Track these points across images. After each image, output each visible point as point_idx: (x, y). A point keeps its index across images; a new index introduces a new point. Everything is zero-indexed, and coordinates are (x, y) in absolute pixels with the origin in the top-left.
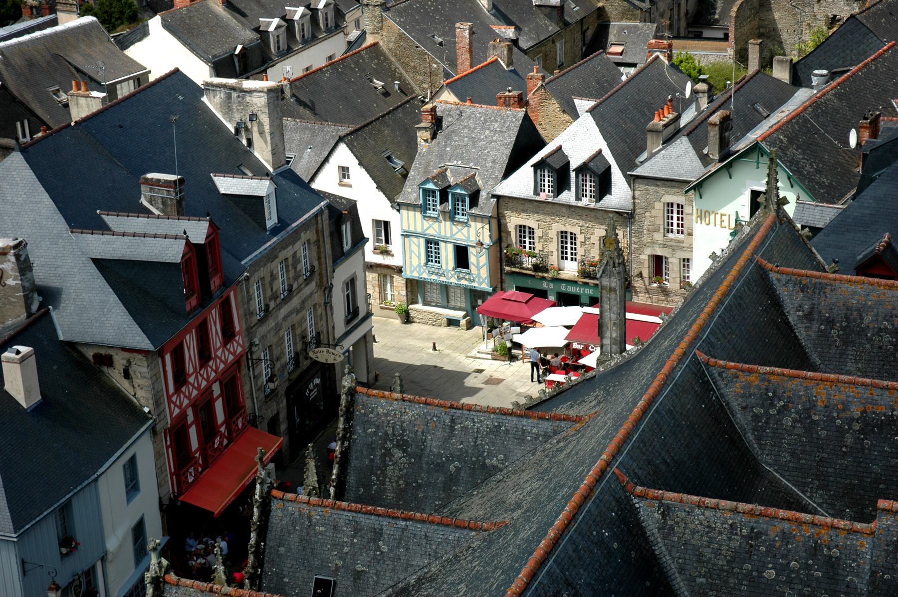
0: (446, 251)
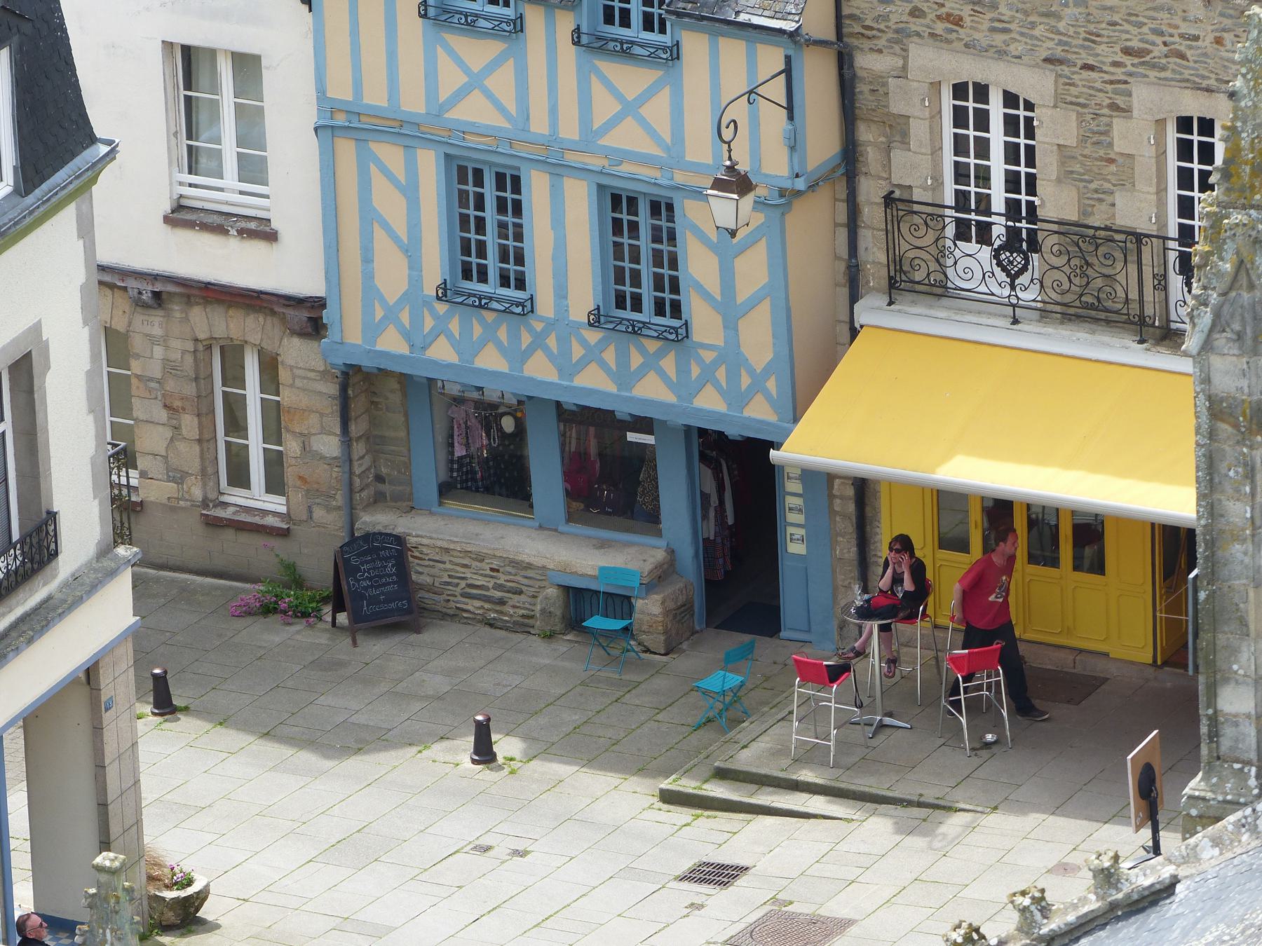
0: (558, 221)
